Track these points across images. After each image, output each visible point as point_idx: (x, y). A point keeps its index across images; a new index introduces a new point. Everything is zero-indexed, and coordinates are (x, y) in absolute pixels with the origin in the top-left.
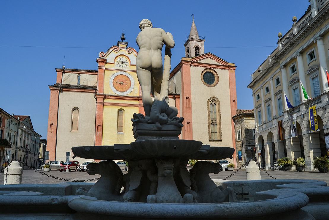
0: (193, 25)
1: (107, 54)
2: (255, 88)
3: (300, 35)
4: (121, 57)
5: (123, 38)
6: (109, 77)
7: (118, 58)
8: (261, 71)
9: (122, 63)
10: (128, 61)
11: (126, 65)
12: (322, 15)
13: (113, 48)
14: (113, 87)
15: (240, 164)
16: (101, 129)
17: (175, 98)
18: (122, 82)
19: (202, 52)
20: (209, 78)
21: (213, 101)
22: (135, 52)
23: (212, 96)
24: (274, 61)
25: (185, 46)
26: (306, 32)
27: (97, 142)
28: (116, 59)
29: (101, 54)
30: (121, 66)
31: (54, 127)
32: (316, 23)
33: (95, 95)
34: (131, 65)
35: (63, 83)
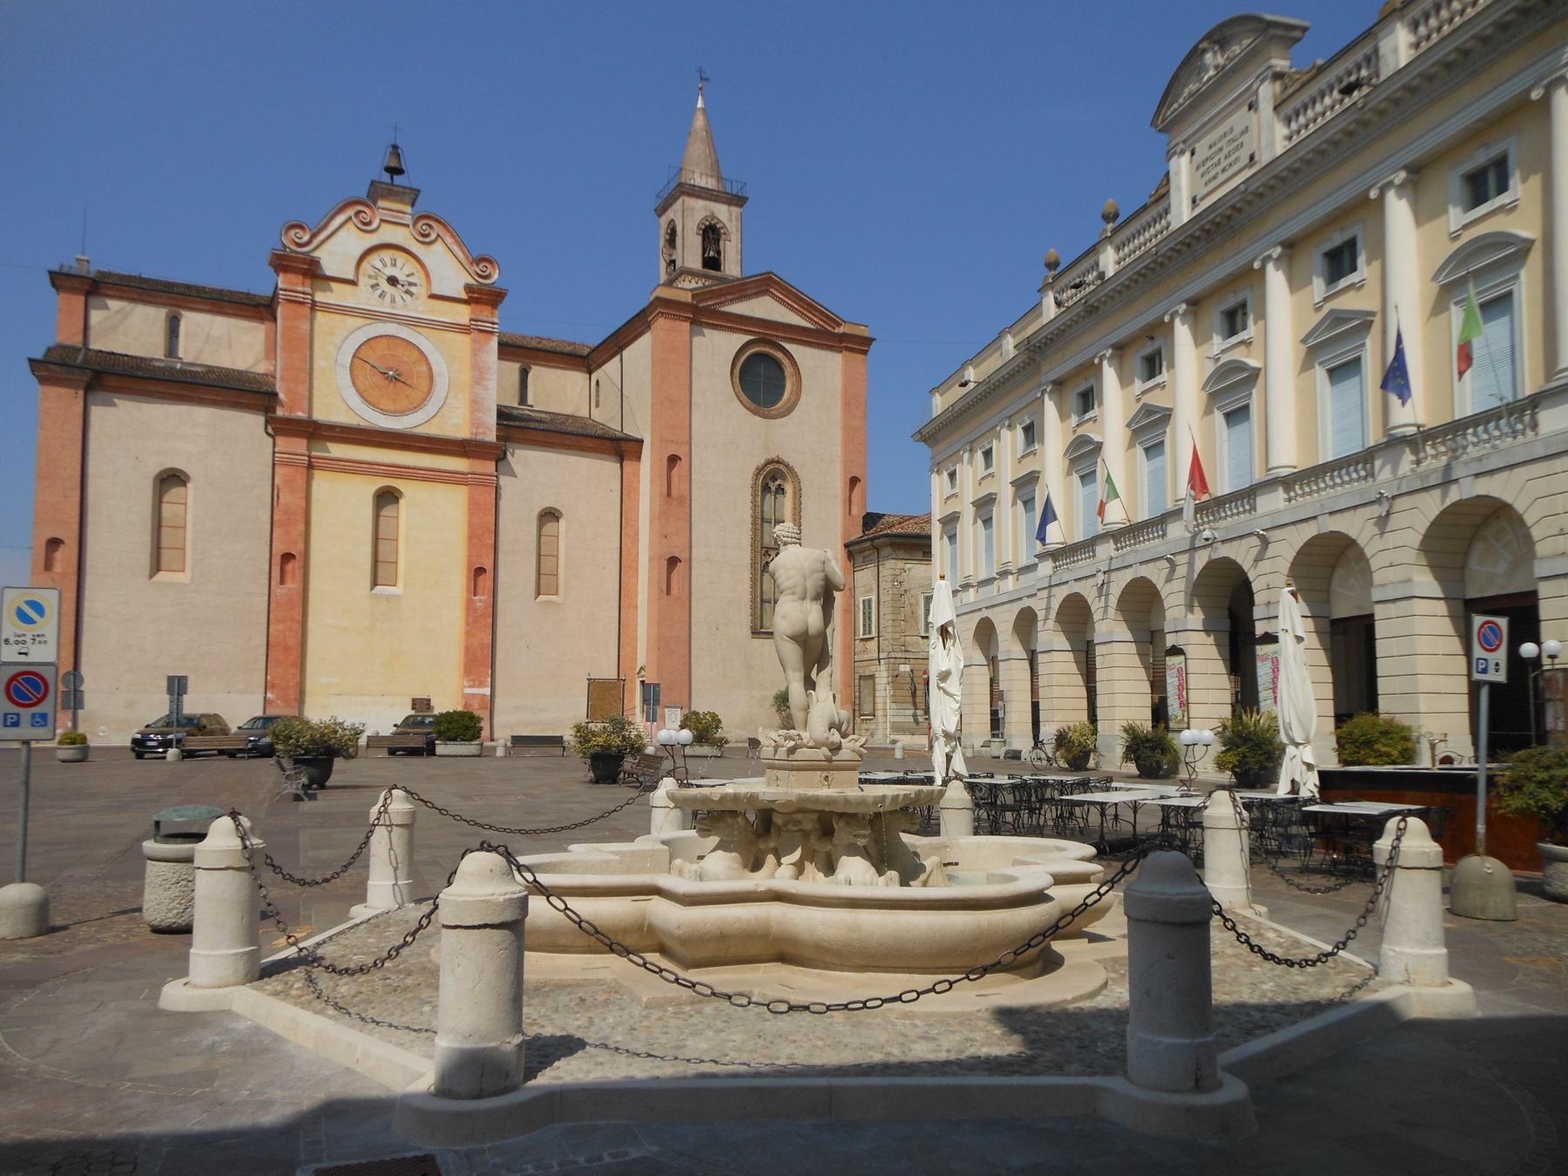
0: (699, 122)
1: (322, 237)
2: (942, 446)
3: (1122, 284)
4: (387, 255)
5: (393, 164)
6: (336, 343)
7: (375, 260)
8: (971, 386)
9: (393, 281)
10: (418, 278)
11: (411, 294)
12: (1202, 229)
13: (350, 212)
14: (353, 391)
15: (864, 726)
16: (299, 573)
17: (621, 457)
18: (391, 371)
19: (732, 267)
20: (762, 380)
21: (772, 478)
22: (449, 240)
23: (773, 456)
24: (1022, 358)
25: (659, 216)
26: (1144, 276)
27: (281, 627)
28: (365, 264)
29: (292, 232)
30: (388, 298)
31: (64, 558)
32: (1179, 251)
33: (267, 422)
34: (433, 297)
35: (95, 345)
